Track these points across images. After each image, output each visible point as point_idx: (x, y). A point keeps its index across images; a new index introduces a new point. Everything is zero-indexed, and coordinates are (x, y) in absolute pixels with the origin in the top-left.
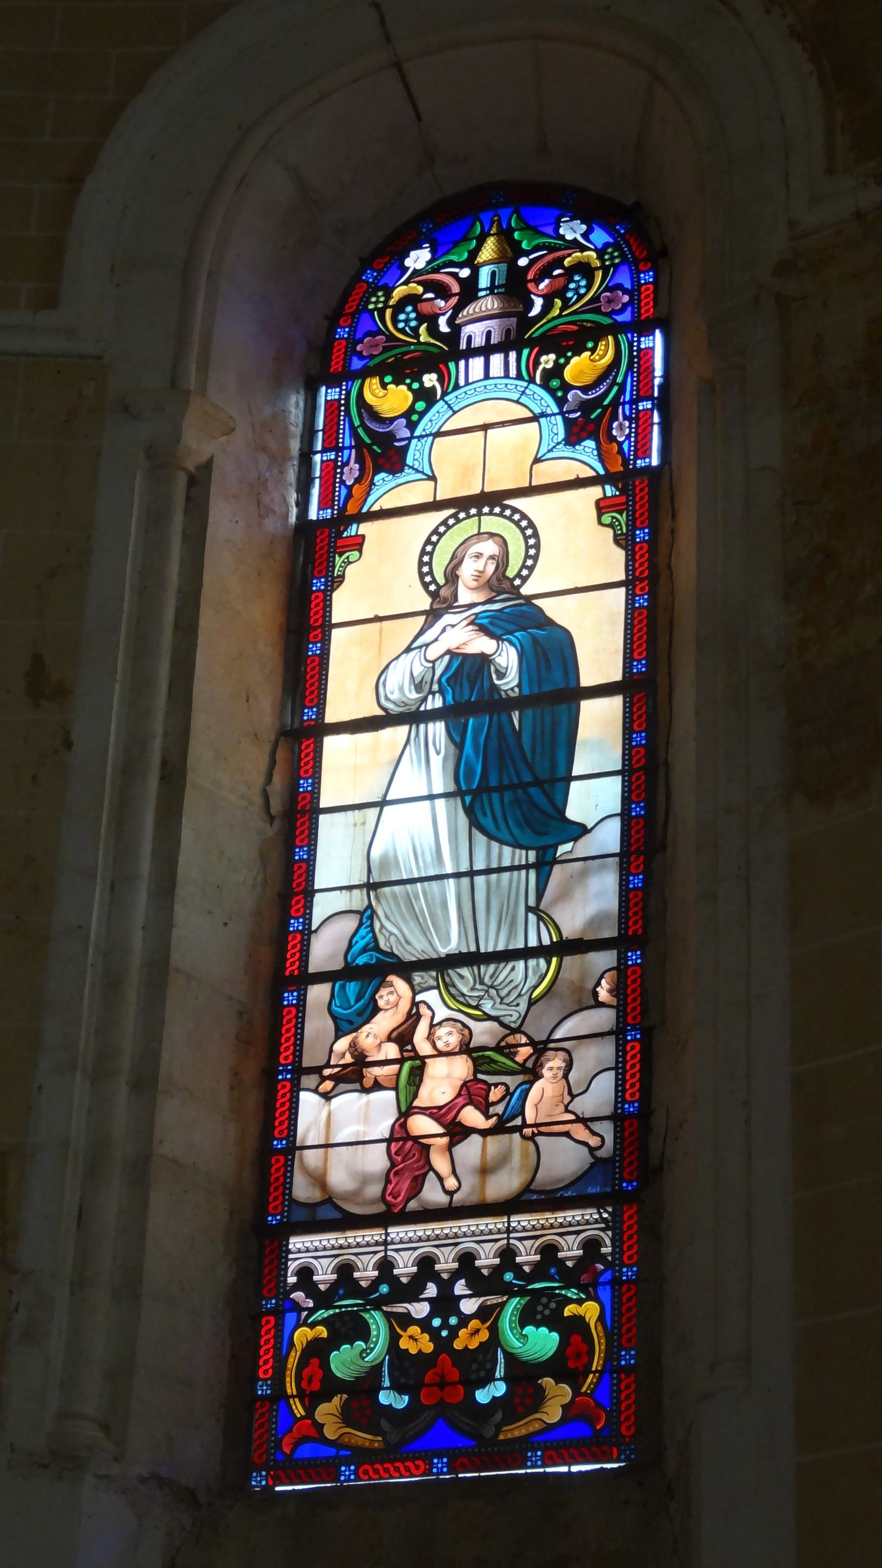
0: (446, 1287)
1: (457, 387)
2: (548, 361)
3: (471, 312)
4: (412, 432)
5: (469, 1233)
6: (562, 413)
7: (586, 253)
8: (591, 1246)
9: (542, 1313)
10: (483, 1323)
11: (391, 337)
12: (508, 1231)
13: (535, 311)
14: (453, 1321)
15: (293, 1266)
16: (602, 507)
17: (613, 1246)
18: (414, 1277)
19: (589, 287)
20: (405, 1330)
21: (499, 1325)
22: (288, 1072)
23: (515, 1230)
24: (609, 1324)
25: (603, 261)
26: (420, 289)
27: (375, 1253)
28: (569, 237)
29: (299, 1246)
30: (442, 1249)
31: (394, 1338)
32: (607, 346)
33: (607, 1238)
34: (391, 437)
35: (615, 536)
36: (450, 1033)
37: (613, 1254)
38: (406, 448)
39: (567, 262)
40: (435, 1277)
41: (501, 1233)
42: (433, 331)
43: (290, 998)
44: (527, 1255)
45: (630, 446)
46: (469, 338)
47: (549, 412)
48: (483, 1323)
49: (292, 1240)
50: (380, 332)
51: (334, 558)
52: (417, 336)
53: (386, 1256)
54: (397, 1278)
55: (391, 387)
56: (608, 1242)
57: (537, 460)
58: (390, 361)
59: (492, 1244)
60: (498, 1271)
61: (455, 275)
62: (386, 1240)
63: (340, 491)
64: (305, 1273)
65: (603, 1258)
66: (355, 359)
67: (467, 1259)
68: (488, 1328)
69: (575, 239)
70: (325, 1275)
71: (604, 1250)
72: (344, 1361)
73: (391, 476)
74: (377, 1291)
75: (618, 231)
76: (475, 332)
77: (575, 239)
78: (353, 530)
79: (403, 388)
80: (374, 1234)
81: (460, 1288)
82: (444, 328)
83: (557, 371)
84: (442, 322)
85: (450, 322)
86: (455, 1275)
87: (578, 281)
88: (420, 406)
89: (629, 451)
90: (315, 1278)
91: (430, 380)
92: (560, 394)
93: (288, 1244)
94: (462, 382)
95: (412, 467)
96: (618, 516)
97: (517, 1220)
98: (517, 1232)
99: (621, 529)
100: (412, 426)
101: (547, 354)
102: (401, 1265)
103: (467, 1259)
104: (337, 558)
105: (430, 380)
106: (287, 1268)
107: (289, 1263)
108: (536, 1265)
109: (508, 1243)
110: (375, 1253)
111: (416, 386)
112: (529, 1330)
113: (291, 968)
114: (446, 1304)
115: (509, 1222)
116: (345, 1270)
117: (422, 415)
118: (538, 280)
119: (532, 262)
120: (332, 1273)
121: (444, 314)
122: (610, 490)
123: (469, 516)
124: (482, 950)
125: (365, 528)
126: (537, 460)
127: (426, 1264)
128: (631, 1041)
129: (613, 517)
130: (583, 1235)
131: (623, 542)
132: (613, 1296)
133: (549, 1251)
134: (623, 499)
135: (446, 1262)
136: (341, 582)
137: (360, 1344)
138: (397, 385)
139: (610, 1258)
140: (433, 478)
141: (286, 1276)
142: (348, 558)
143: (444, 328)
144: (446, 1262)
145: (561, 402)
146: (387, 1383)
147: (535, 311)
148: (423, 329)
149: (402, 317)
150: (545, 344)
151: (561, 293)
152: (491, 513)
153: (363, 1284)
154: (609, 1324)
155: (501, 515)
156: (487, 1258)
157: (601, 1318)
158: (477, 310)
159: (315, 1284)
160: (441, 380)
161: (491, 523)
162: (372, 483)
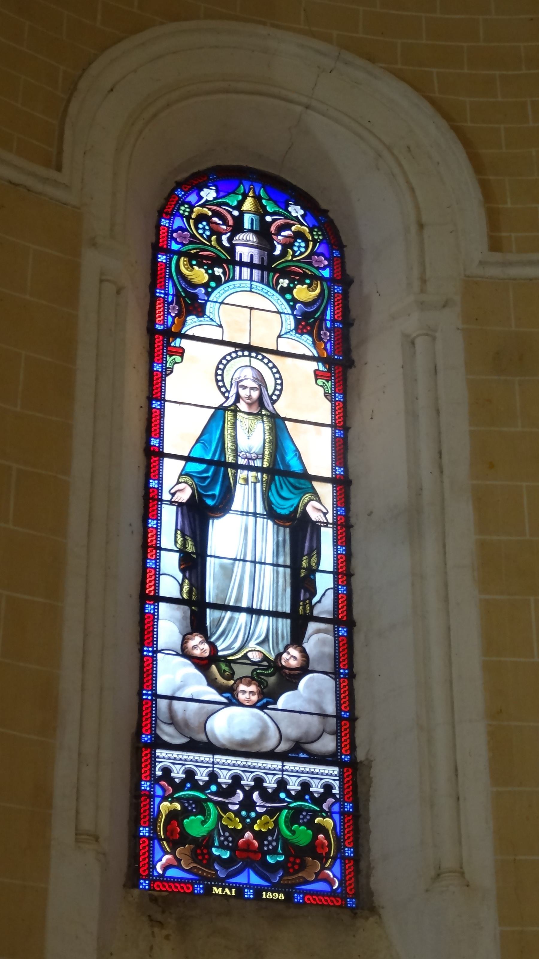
0: (248, 795)
1: (233, 279)
2: (284, 282)
3: (241, 238)
4: (208, 298)
5: (262, 767)
6: (292, 314)
7: (303, 227)
8: (328, 788)
9: (193, 808)
10: (271, 818)
11: (193, 236)
12: (282, 771)
13: (277, 252)
14: (253, 814)
15: (159, 766)
16: (317, 375)
17: (339, 790)
18: (230, 786)
19: (307, 247)
20: (225, 814)
21: (279, 822)
22: (342, 673)
23: (287, 770)
24: (338, 833)
25: (313, 236)
26: (210, 213)
27: (207, 767)
28: (294, 214)
29: (218, 760)
30: (199, 768)
31: (220, 818)
32: (317, 284)
33: (336, 784)
34: (195, 297)
35: (325, 393)
36: (295, 658)
37: (339, 794)
38: (204, 305)
39: (293, 228)
40: (242, 787)
41: (209, 764)
42: (219, 241)
43: (149, 608)
44: (294, 785)
45: (331, 346)
46: (241, 255)
47: (286, 312)
48: (271, 818)
49: (157, 751)
50: (186, 230)
51: (166, 358)
52: (210, 241)
53: (213, 770)
54: (265, 788)
55: (196, 268)
56: (337, 788)
57: (280, 336)
58: (192, 252)
59: (205, 769)
60: (276, 791)
61: (230, 213)
62: (213, 761)
63: (167, 319)
64: (167, 771)
65: (334, 796)
66: (173, 243)
67: (259, 782)
68: (273, 822)
69: (297, 216)
70: (178, 773)
71: (334, 791)
72: (195, 826)
73: (311, 343)
74: (209, 789)
75: (320, 220)
76: (244, 253)
77: (297, 216)
78: (178, 342)
79: (203, 270)
80: (277, 764)
81: (256, 796)
82: (225, 243)
83: (289, 290)
84: (224, 238)
85: (230, 240)
86: (253, 789)
87: (300, 243)
88: (213, 284)
89: (331, 348)
90: (196, 777)
91: (218, 271)
92: (291, 303)
93: (155, 753)
94: (237, 277)
95: (209, 317)
96: (326, 382)
97: (288, 765)
98: (288, 772)
99: (328, 390)
100: (208, 294)
101: (284, 279)
102: (222, 777)
103: (259, 782)
104: (168, 358)
105: (218, 271)
106: (155, 767)
107: (157, 764)
108: (298, 792)
109: (282, 777)
110: (207, 767)
111: (210, 272)
112: (295, 827)
113: (150, 590)
114: (248, 804)
115: (213, 758)
116: (190, 774)
117: (214, 289)
118: (278, 233)
119: (274, 221)
120: (182, 774)
121: (225, 234)
122: (321, 368)
123: (244, 356)
124: (254, 607)
125: (185, 343)
126: (280, 336)
127: (236, 779)
128: (343, 678)
129: (324, 383)
130: (187, 766)
131: (330, 398)
132: (340, 819)
133: (305, 786)
134: (329, 375)
135: (248, 781)
136: (172, 372)
137: (200, 817)
138: (200, 267)
139: (338, 796)
140: (220, 326)
141: (155, 771)
142: (174, 359)
143: (225, 243)
144: (248, 781)
145: (293, 308)
146: (216, 844)
147: (277, 252)
148: (214, 238)
149: (200, 226)
150: (284, 273)
151: (291, 246)
152: (256, 358)
153: (201, 783)
154: (338, 833)
155: (262, 360)
156: (270, 783)
157: (335, 828)
158: (245, 238)
159: (173, 779)
160: (224, 273)
161: (256, 363)
162: (185, 321)
